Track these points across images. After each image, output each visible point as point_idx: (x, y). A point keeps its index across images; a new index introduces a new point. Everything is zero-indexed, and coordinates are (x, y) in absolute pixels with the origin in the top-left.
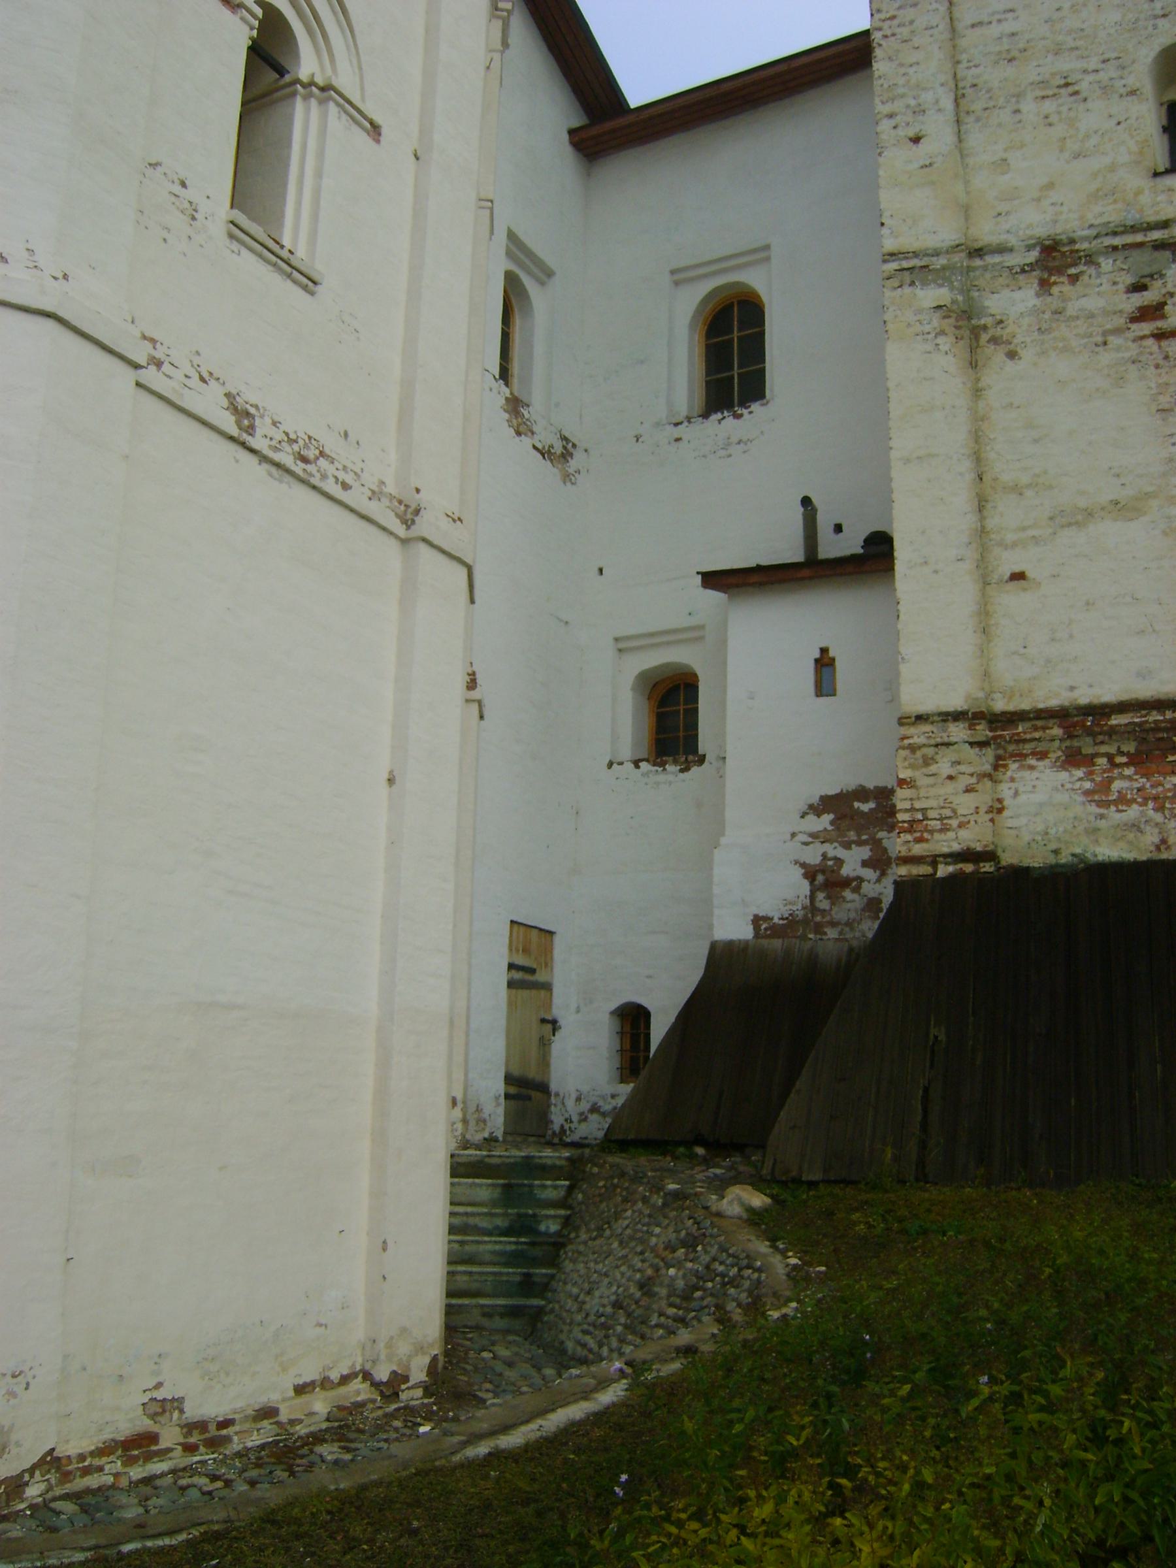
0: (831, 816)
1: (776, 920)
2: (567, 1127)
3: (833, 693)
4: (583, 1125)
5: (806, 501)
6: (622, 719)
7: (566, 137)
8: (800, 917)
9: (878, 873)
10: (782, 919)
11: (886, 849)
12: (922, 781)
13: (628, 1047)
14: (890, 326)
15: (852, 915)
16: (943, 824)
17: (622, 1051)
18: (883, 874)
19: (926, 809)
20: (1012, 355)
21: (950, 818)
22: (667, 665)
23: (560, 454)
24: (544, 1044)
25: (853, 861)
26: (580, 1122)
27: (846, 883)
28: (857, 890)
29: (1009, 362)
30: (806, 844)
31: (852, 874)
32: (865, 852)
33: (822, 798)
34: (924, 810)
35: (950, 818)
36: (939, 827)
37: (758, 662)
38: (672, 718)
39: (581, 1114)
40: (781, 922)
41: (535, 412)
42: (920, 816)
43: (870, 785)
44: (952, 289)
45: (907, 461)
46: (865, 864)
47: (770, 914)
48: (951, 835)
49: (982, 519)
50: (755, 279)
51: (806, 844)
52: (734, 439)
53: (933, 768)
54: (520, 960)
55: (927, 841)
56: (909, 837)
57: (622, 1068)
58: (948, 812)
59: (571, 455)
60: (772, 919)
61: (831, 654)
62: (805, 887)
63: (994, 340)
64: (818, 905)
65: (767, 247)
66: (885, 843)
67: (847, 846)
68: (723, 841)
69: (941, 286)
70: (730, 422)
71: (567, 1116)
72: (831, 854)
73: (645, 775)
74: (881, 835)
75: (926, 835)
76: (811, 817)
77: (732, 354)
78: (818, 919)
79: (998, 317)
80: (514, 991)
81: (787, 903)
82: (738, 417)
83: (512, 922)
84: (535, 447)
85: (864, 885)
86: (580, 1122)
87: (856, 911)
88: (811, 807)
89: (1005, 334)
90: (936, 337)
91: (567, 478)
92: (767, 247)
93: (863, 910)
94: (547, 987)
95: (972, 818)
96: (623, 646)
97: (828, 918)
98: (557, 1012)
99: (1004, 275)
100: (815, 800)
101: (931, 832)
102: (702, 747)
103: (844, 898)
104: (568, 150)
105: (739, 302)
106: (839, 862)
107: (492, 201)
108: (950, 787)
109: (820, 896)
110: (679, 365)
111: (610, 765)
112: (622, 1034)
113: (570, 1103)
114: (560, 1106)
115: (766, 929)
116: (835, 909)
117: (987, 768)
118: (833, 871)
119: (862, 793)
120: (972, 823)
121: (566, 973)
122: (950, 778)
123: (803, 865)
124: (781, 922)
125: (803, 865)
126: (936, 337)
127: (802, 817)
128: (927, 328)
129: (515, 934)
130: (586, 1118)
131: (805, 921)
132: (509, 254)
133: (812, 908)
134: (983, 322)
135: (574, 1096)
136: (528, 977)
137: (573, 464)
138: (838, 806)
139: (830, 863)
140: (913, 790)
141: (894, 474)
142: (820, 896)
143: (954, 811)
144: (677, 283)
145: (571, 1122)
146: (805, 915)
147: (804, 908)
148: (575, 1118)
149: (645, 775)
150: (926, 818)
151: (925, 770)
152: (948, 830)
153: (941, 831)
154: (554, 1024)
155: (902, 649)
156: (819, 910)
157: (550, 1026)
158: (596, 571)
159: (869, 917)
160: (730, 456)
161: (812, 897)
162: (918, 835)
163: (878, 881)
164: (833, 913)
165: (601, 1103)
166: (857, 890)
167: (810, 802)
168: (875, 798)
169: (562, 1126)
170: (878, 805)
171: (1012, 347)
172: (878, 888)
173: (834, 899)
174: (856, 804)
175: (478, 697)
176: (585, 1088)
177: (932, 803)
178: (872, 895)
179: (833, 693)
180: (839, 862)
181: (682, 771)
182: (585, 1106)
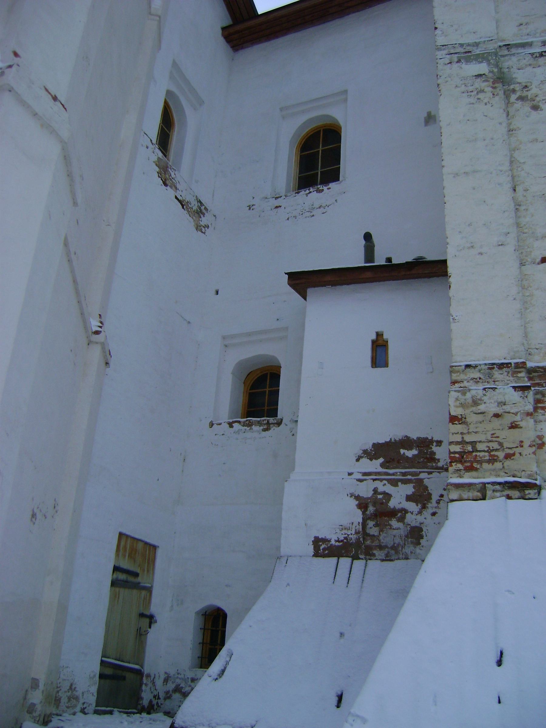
0: (381, 460)
1: (333, 542)
2: (155, 702)
3: (386, 365)
4: (168, 701)
5: (368, 237)
6: (223, 393)
7: (220, 32)
8: (353, 540)
9: (420, 506)
10: (338, 541)
11: (426, 488)
12: (472, 418)
13: (208, 641)
14: (441, 86)
15: (397, 540)
16: (490, 456)
17: (203, 643)
18: (424, 507)
19: (475, 442)
20: (535, 108)
21: (497, 450)
22: (259, 356)
23: (197, 211)
24: (141, 635)
25: (399, 496)
26: (165, 699)
27: (392, 513)
28: (402, 519)
29: (534, 113)
30: (360, 481)
31: (398, 507)
32: (409, 489)
33: (374, 445)
34: (473, 443)
35: (497, 450)
36: (487, 458)
37: (329, 341)
38: (260, 394)
39: (167, 692)
40: (337, 544)
41: (182, 175)
42: (470, 448)
43: (414, 436)
44: (489, 64)
45: (456, 175)
46: (409, 498)
47: (328, 537)
48: (498, 465)
49: (517, 217)
50: (337, 114)
51: (360, 481)
52: (317, 205)
53: (482, 408)
54: (125, 564)
55: (476, 469)
56: (460, 466)
57: (202, 658)
58: (496, 446)
59: (204, 214)
60: (329, 541)
61: (385, 337)
62: (358, 517)
63: (521, 98)
64: (368, 531)
65: (346, 92)
66: (426, 482)
67: (394, 483)
68: (293, 476)
69: (481, 62)
70: (314, 195)
71: (156, 693)
72: (381, 489)
73: (238, 432)
74: (422, 476)
75: (475, 465)
76: (365, 461)
77: (319, 157)
78: (368, 542)
79: (524, 84)
80: (117, 589)
81: (343, 528)
82: (319, 191)
83: (121, 535)
84: (176, 198)
85: (408, 516)
86: (165, 699)
87: (401, 537)
88: (365, 452)
89: (530, 94)
90: (477, 93)
91: (199, 228)
92: (346, 92)
93: (406, 536)
94: (149, 590)
95: (518, 450)
96: (228, 342)
97: (376, 543)
98: (154, 609)
99: (527, 59)
100: (369, 446)
101: (480, 462)
102: (281, 413)
103: (391, 525)
104: (222, 40)
105: (324, 131)
106: (388, 496)
107: (160, 17)
108: (496, 423)
109: (371, 523)
110: (282, 163)
111: (212, 425)
112: (204, 629)
113: (159, 682)
114: (150, 685)
115: (324, 549)
116: (383, 535)
117: (530, 408)
118: (382, 503)
119: (407, 443)
120: (517, 455)
121: (164, 579)
122: (497, 416)
123: (357, 498)
124: (337, 544)
125: (357, 498)
126: (477, 93)
127: (358, 460)
128: (471, 88)
129: (123, 543)
130: (171, 696)
131: (358, 544)
132: (172, 77)
133: (364, 533)
134: (512, 87)
135: (163, 677)
136: (131, 579)
137: (204, 221)
138: (387, 452)
139: (380, 497)
140: (464, 426)
141: (445, 184)
142: (371, 523)
143: (501, 444)
144: (283, 117)
145: (159, 698)
146: (358, 540)
147: (357, 533)
148: (162, 695)
149: (238, 432)
150: (475, 450)
151: (474, 409)
152: (496, 461)
153: (489, 461)
154: (151, 619)
155: (452, 311)
156: (368, 535)
157: (147, 620)
158: (214, 292)
159: (412, 543)
160: (313, 216)
161: (364, 524)
162: (468, 464)
163: (420, 513)
164: (381, 538)
165: (182, 685)
166: (402, 519)
167: (365, 448)
168: (418, 446)
169: (151, 701)
170: (420, 452)
171: (535, 103)
172: (420, 518)
173: (382, 527)
174: (402, 451)
175: (103, 340)
176: (172, 672)
177: (482, 438)
178: (413, 524)
179: (386, 365)
180: (388, 496)
181: (264, 430)
182: (171, 686)
